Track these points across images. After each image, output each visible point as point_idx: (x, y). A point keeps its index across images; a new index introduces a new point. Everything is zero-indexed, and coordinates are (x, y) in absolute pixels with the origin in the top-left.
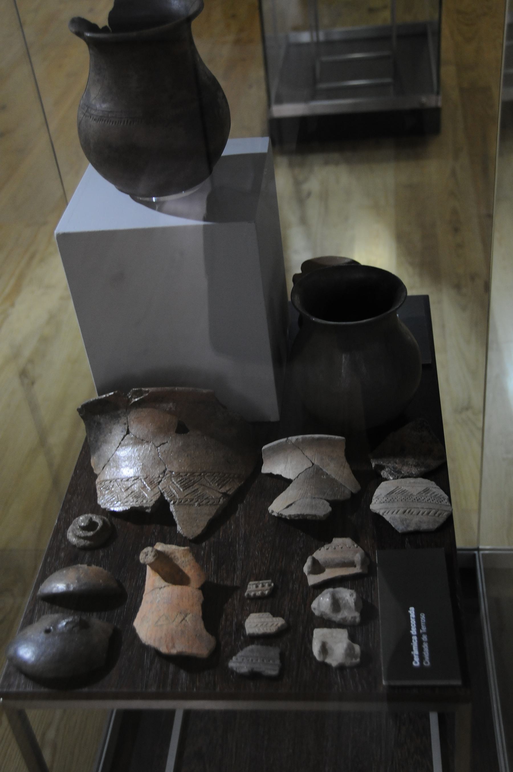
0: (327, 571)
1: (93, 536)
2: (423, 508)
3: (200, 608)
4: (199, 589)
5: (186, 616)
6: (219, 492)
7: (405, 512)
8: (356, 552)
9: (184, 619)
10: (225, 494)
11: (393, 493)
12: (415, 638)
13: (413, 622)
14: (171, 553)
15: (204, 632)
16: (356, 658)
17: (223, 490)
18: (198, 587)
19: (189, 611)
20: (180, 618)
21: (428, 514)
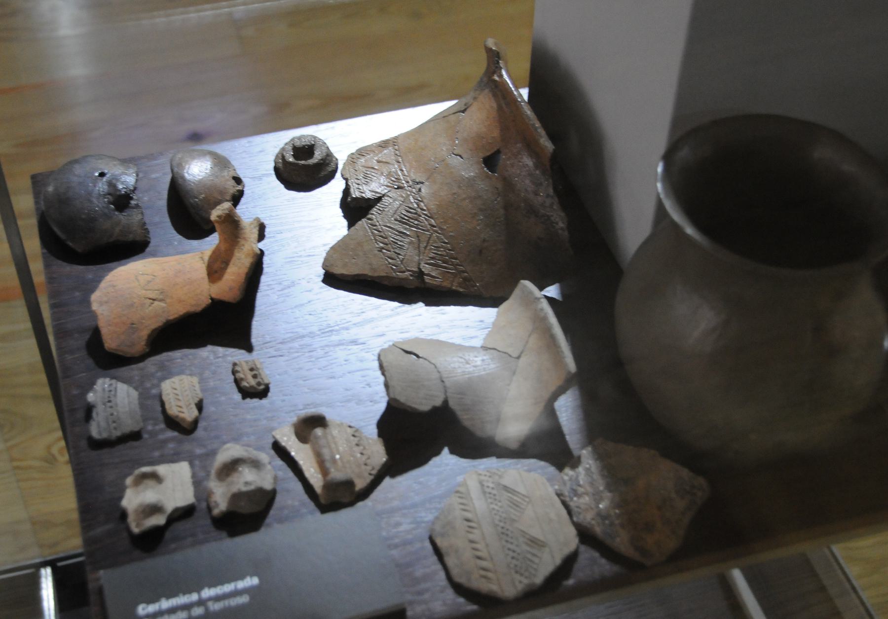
0: (307, 447)
1: (290, 163)
2: (487, 545)
3: (181, 313)
4: (212, 299)
5: (161, 300)
6: (419, 264)
7: (468, 520)
8: (100, 433)
9: (154, 300)
10: (420, 274)
11: (509, 492)
12: (194, 597)
13: (228, 588)
14: (245, 239)
15: (145, 333)
16: (138, 525)
17: (426, 268)
18: (214, 296)
19: (168, 301)
20: (153, 295)
21: (479, 558)
